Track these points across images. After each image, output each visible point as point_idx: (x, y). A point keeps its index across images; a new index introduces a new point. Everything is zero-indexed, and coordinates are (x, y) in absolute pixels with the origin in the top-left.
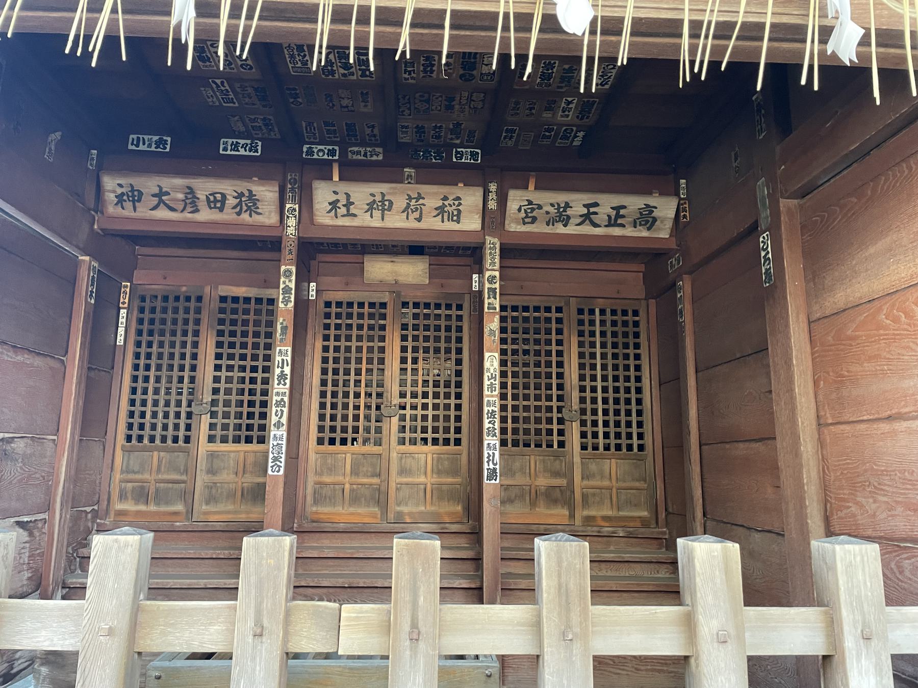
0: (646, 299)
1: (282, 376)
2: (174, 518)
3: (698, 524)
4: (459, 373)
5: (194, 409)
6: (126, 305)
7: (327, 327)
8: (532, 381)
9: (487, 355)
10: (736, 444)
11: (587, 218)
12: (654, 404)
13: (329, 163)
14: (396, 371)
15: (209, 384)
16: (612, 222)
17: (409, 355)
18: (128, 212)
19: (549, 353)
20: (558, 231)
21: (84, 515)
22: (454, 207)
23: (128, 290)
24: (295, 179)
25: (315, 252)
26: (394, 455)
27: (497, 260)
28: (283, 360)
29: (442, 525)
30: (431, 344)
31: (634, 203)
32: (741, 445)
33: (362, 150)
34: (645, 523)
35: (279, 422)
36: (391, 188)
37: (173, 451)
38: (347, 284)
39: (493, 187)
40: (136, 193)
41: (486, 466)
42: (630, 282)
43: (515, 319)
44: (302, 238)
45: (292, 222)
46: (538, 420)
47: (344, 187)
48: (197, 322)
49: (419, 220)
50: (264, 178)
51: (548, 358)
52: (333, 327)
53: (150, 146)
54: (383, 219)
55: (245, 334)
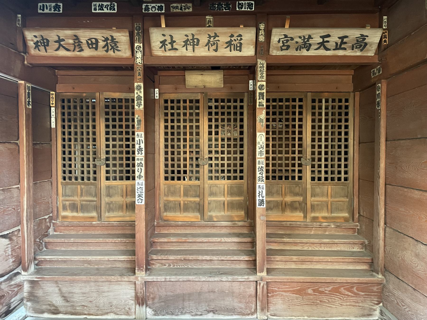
0: (354, 92)
1: (140, 149)
2: (92, 220)
3: (381, 229)
5: (97, 163)
6: (54, 105)
7: (166, 114)
8: (284, 143)
9: (258, 134)
10: (413, 191)
11: (322, 45)
12: (355, 154)
13: (158, 15)
15: (103, 149)
16: (338, 47)
17: (213, 130)
18: (42, 53)
19: (294, 126)
20: (303, 54)
21: (44, 220)
22: (237, 41)
23: (54, 96)
24: (139, 27)
25: (153, 73)
26: (206, 186)
27: (265, 75)
28: (140, 140)
29: (234, 223)
30: (226, 117)
31: (354, 34)
32: (417, 192)
33: (179, 5)
34: (346, 220)
35: (140, 175)
36: (198, 31)
37: (87, 184)
38: (176, 89)
39: (262, 26)
40: (45, 41)
41: (257, 198)
42: (345, 81)
43: (274, 107)
44: (146, 64)
45: (139, 55)
46: (287, 165)
47: (169, 32)
48: (94, 114)
49: (216, 50)
50: (120, 28)
51: (294, 129)
52: (169, 115)
53: (50, 10)
54: (194, 51)
55: (121, 120)
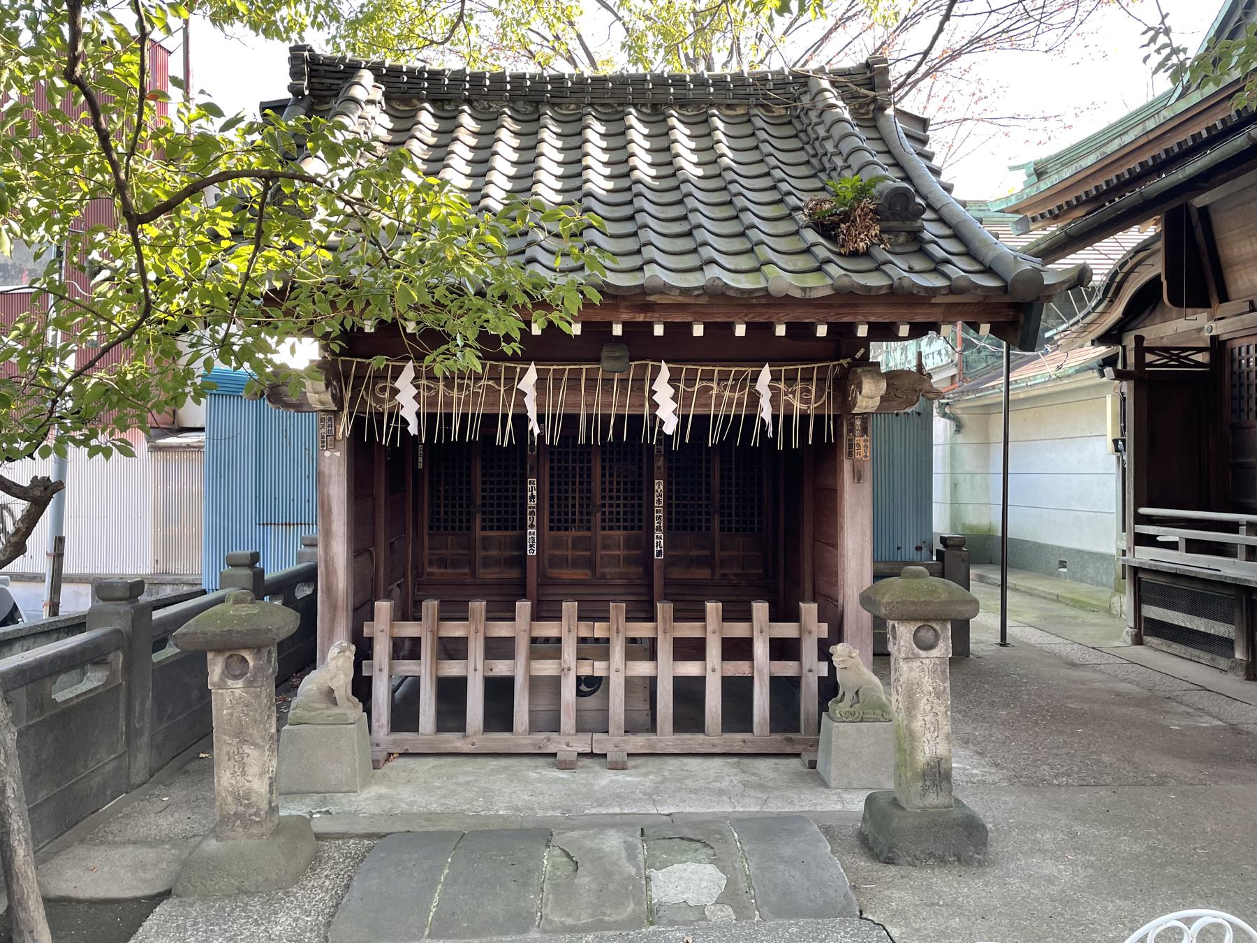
1: (532, 497)
4: (640, 475)
14: (599, 483)
26: (599, 537)
